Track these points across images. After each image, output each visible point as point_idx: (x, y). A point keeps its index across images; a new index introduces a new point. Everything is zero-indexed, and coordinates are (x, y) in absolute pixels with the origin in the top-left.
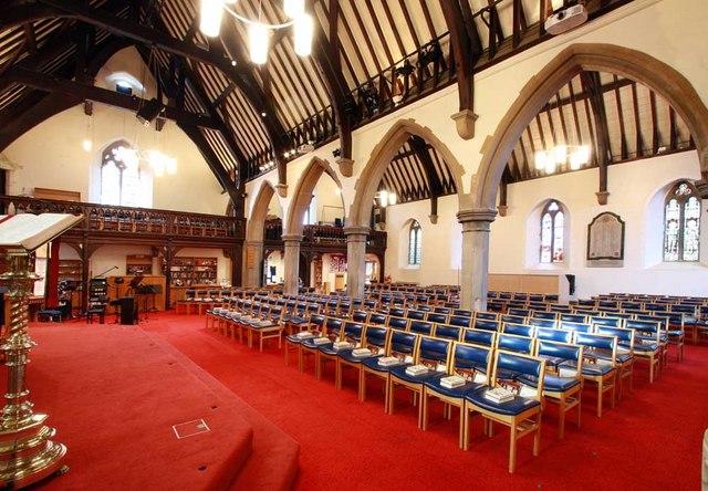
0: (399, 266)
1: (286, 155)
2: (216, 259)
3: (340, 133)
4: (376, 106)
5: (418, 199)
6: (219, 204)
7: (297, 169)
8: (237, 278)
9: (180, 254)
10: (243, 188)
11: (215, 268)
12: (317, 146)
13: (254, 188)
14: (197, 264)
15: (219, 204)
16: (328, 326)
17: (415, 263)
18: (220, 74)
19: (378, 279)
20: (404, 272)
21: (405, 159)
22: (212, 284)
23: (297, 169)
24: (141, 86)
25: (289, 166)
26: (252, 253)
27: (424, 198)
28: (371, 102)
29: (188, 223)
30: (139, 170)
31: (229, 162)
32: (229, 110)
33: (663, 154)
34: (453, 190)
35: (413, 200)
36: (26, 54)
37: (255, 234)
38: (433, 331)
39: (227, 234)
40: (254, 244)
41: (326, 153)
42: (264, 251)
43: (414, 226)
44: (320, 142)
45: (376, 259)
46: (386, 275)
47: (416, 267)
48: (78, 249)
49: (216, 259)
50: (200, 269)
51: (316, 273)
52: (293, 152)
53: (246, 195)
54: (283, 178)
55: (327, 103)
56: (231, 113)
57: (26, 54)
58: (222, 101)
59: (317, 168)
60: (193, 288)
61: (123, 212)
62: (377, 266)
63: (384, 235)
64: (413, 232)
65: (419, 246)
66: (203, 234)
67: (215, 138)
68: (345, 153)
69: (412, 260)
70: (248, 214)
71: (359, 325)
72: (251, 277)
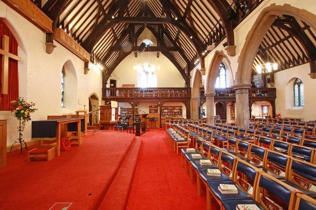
0: (286, 107)
1: (203, 54)
2: (182, 106)
3: (226, 35)
4: (247, 8)
5: (299, 64)
6: (182, 84)
7: (209, 60)
8: (188, 116)
9: (165, 105)
10: (189, 74)
11: (181, 110)
12: (216, 45)
13: (193, 73)
14: (174, 109)
15: (182, 84)
16: (239, 145)
17: (299, 105)
18: (175, 27)
19: (271, 116)
20: (290, 111)
21: (274, 42)
22: (180, 117)
23: (209, 60)
24: (152, 43)
25: (206, 59)
26: (194, 104)
27: (304, 63)
28: (243, 7)
29: (173, 92)
30: (63, 72)
31: (184, 65)
32: (181, 42)
33: (292, 67)
34: (43, 156)
35: (294, 65)
36: (116, 41)
37: (195, 94)
38: (298, 123)
39: (183, 95)
40: (195, 99)
41: (220, 48)
42: (200, 103)
43: (297, 82)
44: (217, 43)
45: (269, 104)
46: (277, 112)
47: (299, 108)
48: (131, 104)
49: (182, 106)
50: (175, 111)
51: (231, 112)
52: (206, 51)
53: (190, 77)
54: (203, 66)
55: (218, 18)
56: (181, 43)
57: (116, 41)
58: (177, 38)
59: (219, 56)
60: (172, 119)
61: (150, 90)
62: (271, 107)
63: (274, 90)
64: (296, 86)
65: (302, 98)
66: (135, 107)
67: (177, 55)
68: (231, 42)
69: (297, 104)
70: (192, 86)
71: (262, 149)
72: (195, 114)
